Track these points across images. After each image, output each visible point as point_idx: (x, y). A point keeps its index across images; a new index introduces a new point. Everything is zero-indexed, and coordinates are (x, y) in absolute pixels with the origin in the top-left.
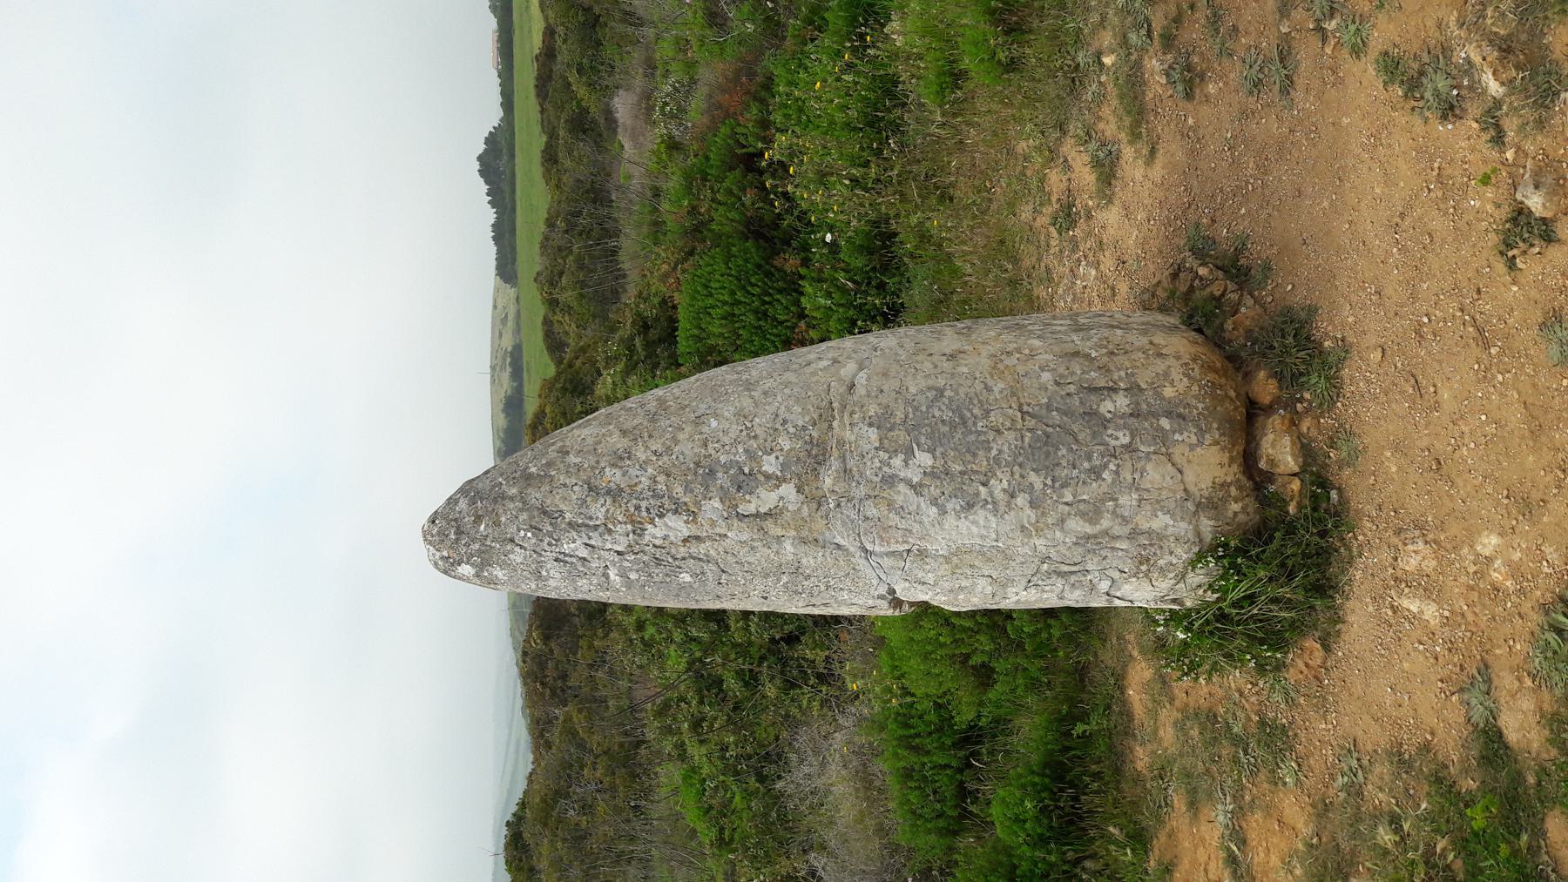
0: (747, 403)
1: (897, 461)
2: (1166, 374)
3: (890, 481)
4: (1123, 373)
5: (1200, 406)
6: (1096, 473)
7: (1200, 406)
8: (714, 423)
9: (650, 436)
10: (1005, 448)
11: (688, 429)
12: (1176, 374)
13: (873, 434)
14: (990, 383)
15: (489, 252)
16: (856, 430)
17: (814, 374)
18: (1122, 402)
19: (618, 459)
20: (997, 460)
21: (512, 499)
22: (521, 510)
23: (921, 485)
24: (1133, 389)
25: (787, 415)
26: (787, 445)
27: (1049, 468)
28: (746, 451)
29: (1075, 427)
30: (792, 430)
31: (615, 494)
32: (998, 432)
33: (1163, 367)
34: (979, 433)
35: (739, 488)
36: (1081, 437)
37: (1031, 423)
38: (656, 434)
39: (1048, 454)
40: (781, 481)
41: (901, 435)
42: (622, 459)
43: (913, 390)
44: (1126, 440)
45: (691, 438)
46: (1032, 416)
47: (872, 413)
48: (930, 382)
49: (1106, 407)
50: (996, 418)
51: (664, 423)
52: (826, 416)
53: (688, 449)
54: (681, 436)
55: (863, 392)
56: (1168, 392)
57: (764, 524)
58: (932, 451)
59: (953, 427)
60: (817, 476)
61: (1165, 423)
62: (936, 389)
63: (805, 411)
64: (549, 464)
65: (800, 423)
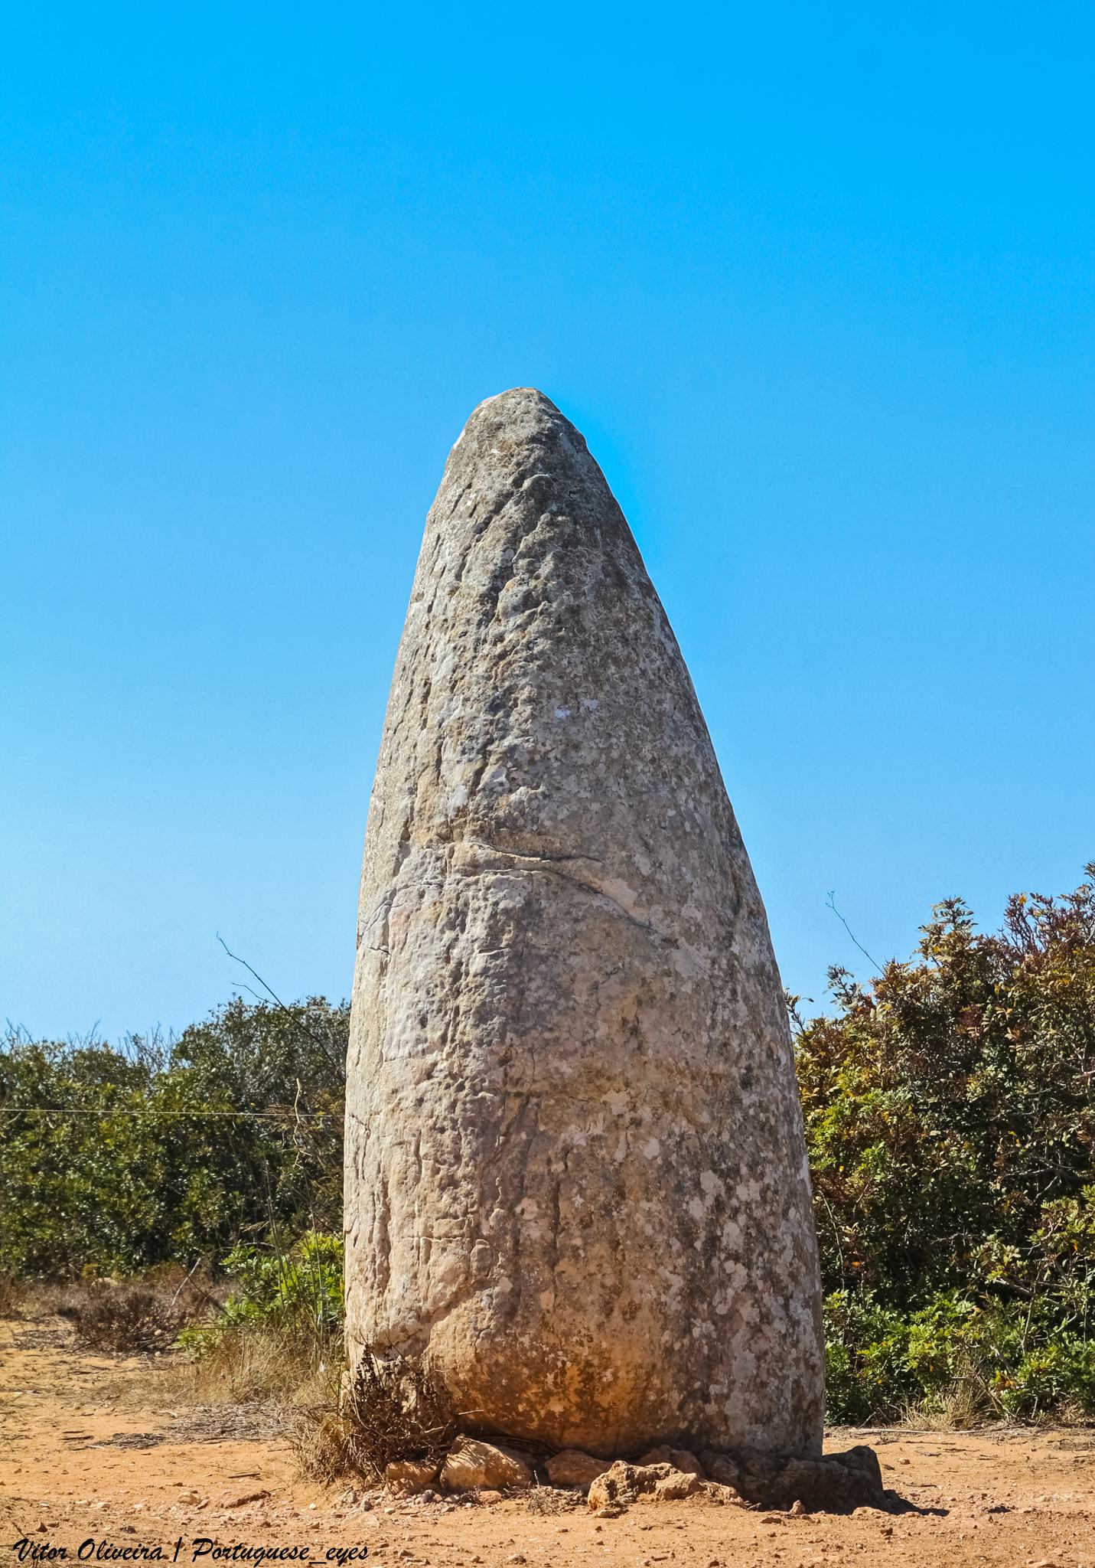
8: (561, 714)
15: (579, 429)
18: (535, 1231)
24: (552, 1254)
49: (528, 1207)
57: (430, 770)
58: (485, 972)
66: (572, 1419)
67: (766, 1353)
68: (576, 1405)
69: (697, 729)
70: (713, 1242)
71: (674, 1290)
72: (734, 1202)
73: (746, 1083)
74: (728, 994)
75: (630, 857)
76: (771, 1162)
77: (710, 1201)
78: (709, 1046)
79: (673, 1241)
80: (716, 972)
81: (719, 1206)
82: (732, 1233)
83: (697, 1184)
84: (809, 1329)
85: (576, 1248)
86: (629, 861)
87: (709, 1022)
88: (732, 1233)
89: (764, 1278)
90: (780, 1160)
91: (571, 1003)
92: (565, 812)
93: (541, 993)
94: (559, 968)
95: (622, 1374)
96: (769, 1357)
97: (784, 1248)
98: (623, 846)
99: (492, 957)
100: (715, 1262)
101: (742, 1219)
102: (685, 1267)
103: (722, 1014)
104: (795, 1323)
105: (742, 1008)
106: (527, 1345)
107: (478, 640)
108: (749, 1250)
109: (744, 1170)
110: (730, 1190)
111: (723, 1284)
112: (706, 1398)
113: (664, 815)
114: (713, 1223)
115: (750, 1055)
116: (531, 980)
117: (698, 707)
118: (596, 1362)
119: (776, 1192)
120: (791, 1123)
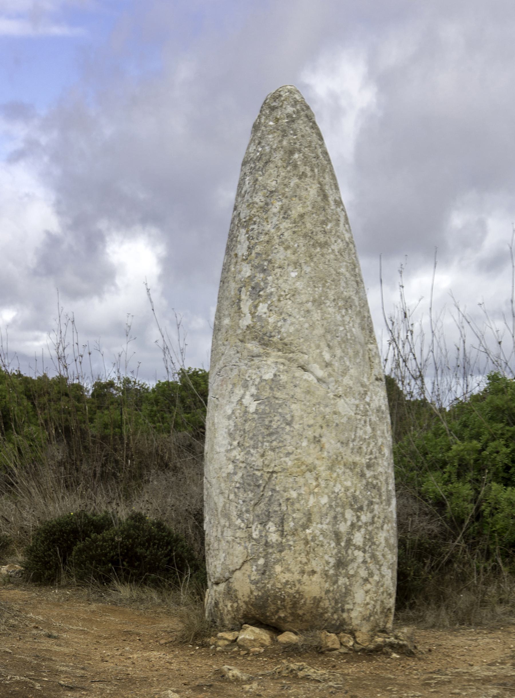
0: (304, 298)
1: (253, 390)
2: (289, 570)
3: (246, 386)
4: (291, 543)
5: (269, 586)
6: (240, 516)
7: (269, 586)
9: (294, 232)
10: (254, 459)
11: (293, 257)
12: (288, 576)
13: (268, 376)
14: (292, 457)
16: (273, 365)
17: (318, 347)
18: (274, 538)
19: (285, 213)
20: (248, 453)
21: (280, 142)
22: (271, 148)
23: (242, 404)
25: (289, 322)
26: (271, 320)
27: (244, 486)
28: (271, 293)
29: (262, 505)
30: (279, 324)
31: (265, 208)
32: (263, 456)
33: (293, 570)
34: (262, 443)
35: (253, 288)
36: (257, 508)
37: (266, 476)
38: (295, 236)
39: (249, 485)
40: (253, 314)
41: (266, 394)
42: (285, 213)
43: (293, 406)
44: (254, 536)
45: (286, 258)
46: (270, 478)
47: (282, 377)
48: (297, 419)
49: (271, 527)
50: (270, 454)
51: (302, 241)
52: (285, 347)
53: (280, 255)
54: (289, 252)
55: (297, 374)
56: (278, 568)
57: (235, 305)
58: (256, 412)
59: (268, 427)
60: (253, 339)
61: (261, 561)
62: (292, 421)
63: (289, 334)
64: (295, 166)
65: (283, 330)
66: (288, 620)
67: (369, 590)
68: (290, 613)
69: (357, 282)
70: (349, 541)
71: (331, 565)
72: (360, 523)
73: (369, 466)
74: (362, 422)
75: (321, 352)
76: (378, 504)
77: (349, 523)
78: (353, 449)
79: (332, 542)
80: (358, 412)
81: (353, 525)
82: (358, 538)
83: (343, 514)
84: (389, 578)
85: (291, 546)
86: (321, 355)
87: (353, 437)
88: (358, 538)
89: (370, 558)
90: (382, 503)
91: (292, 429)
92: (293, 328)
93: (279, 423)
94: (287, 410)
95: (308, 602)
96: (370, 592)
97: (381, 543)
98: (318, 347)
99: (259, 404)
100: (350, 552)
101: (363, 530)
102: (336, 554)
103: (360, 433)
104: (383, 576)
105: (368, 429)
106: (270, 588)
107: (259, 233)
108: (365, 544)
109: (365, 508)
110: (358, 518)
111: (352, 561)
112: (343, 611)
113: (338, 330)
114: (350, 533)
115: (371, 453)
116: (275, 416)
117: (360, 270)
118: (297, 596)
119: (379, 518)
120: (388, 484)
